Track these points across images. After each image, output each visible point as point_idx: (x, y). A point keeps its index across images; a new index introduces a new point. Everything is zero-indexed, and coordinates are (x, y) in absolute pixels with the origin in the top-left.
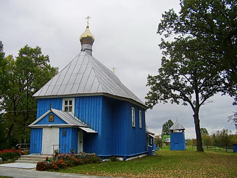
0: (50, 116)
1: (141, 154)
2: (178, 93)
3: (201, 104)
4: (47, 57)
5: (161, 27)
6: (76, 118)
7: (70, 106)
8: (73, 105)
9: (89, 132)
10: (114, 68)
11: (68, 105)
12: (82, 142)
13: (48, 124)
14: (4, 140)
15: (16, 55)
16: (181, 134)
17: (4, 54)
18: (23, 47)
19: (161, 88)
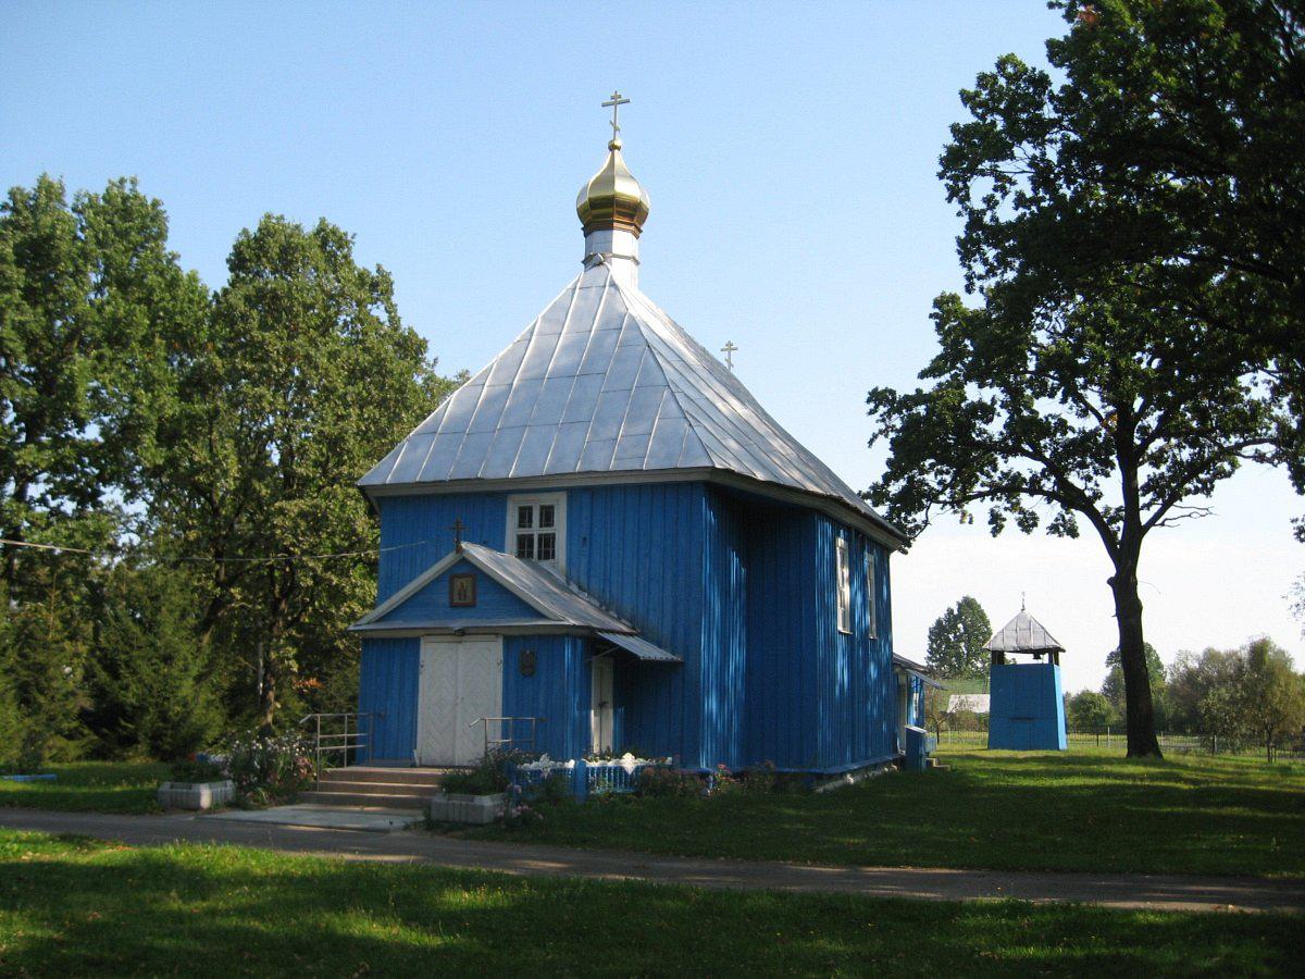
1: (468, 882)
2: (1025, 466)
3: (1152, 522)
6: (574, 588)
8: (560, 529)
10: (730, 347)
12: (610, 704)
16: (1040, 680)
19: (936, 444)
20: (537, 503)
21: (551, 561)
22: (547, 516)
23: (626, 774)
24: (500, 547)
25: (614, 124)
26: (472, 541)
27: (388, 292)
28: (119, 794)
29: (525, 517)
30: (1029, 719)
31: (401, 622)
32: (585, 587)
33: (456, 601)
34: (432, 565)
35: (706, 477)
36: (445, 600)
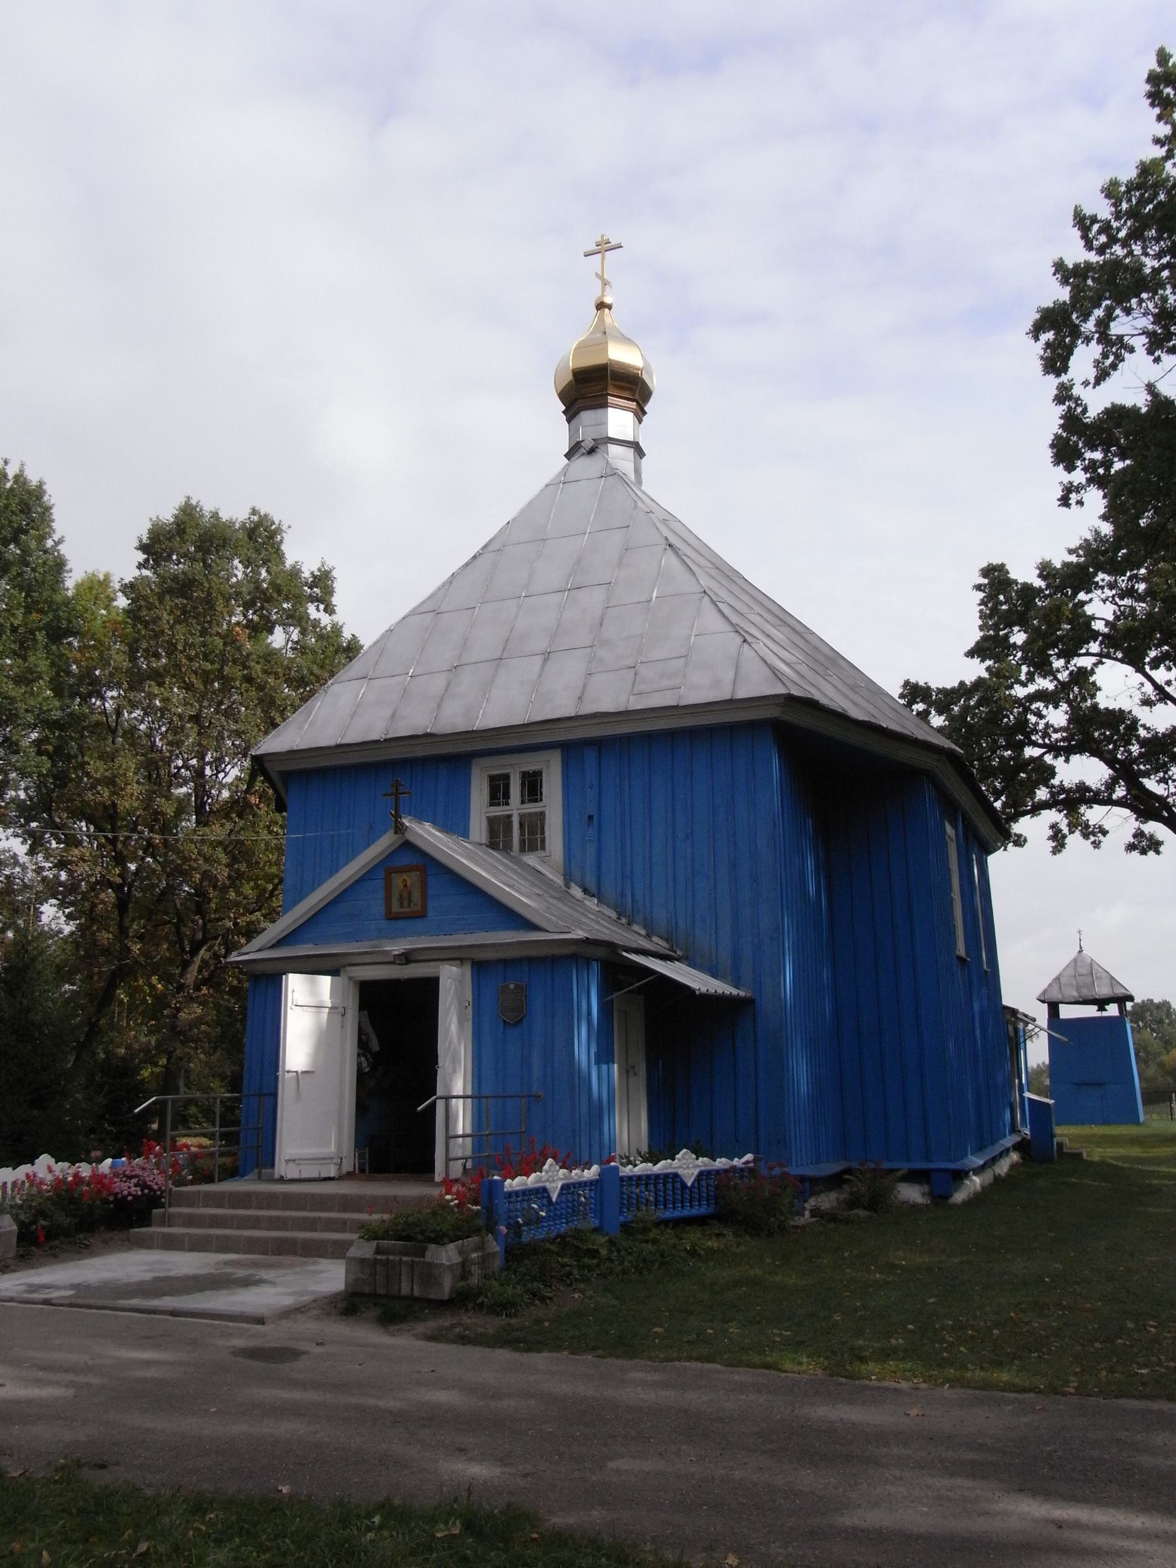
0: (398, 880)
4: (323, 581)
6: (577, 892)
7: (531, 808)
9: (704, 990)
11: (516, 807)
14: (53, 1075)
15: (124, 565)
17: (60, 565)
18: (167, 514)
20: (515, 769)
21: (540, 853)
22: (533, 787)
24: (464, 833)
25: (600, 277)
26: (420, 817)
27: (329, 591)
28: (479, 1118)
29: (498, 791)
30: (1101, 1084)
31: (310, 946)
32: (593, 889)
33: (396, 908)
35: (774, 713)
36: (379, 908)
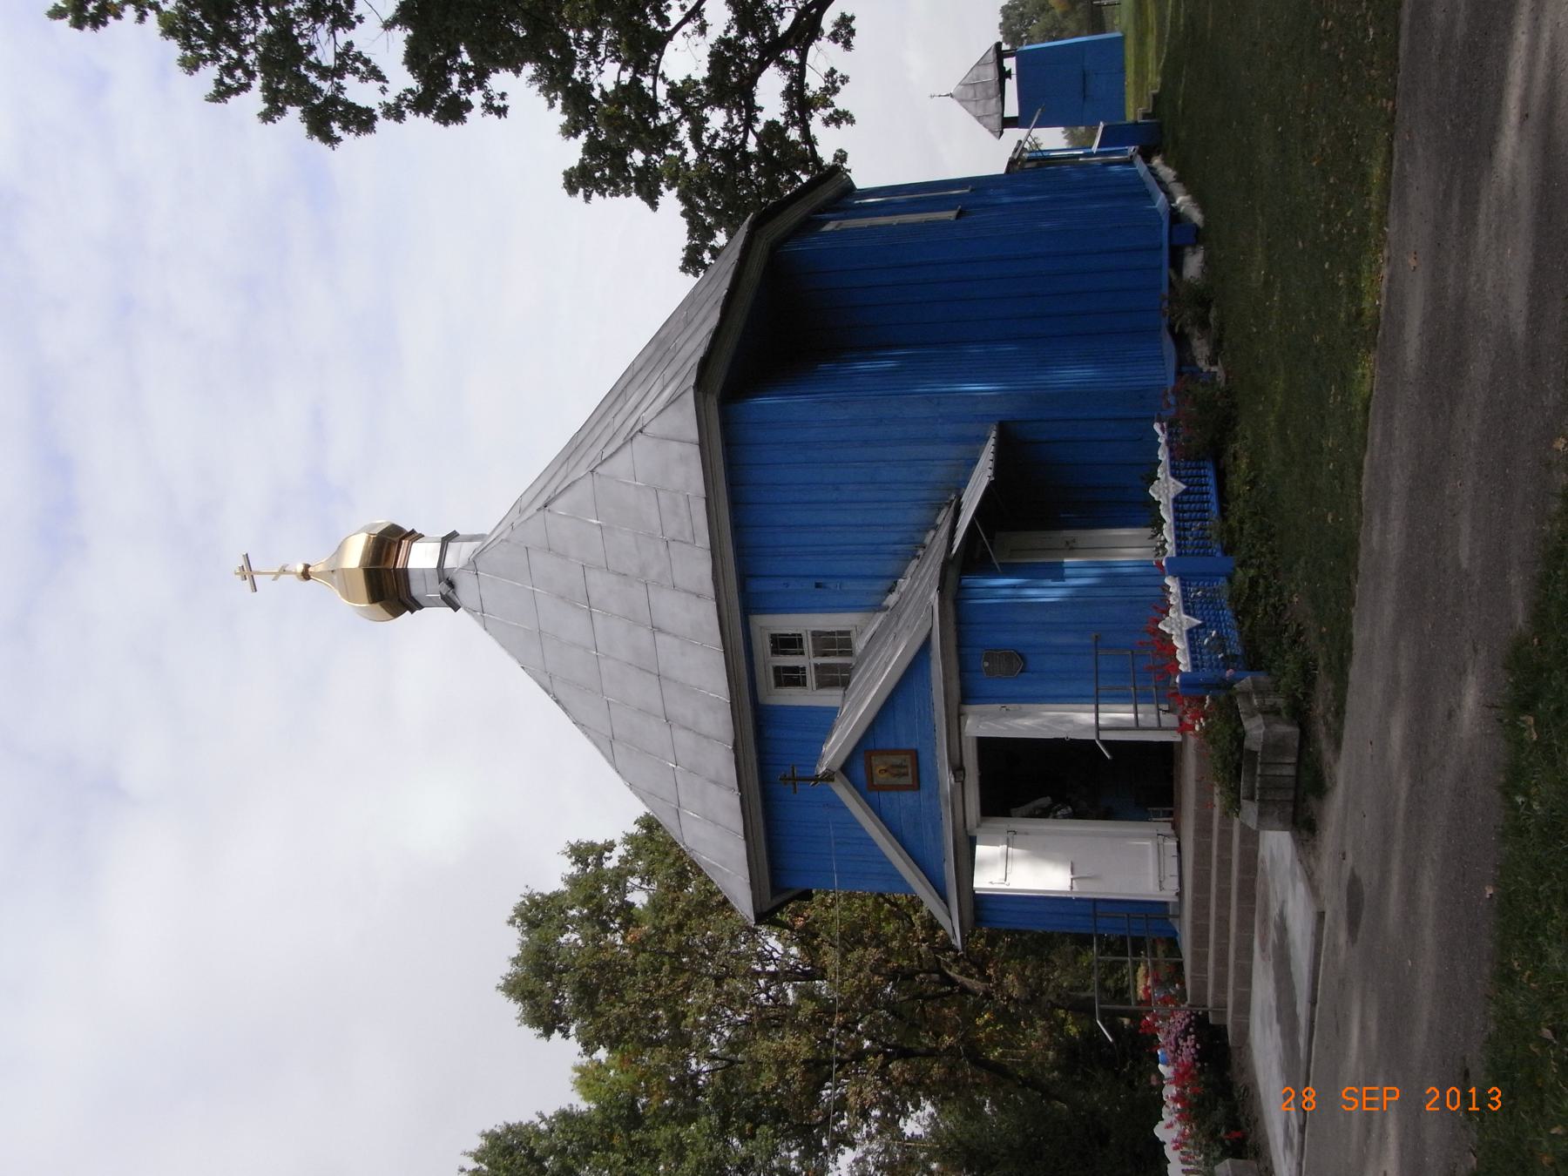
0: (881, 778)
2: (770, 90)
5: (330, 118)
6: (892, 599)
7: (808, 645)
9: (990, 472)
11: (807, 660)
13: (935, 792)
15: (564, 1054)
17: (565, 1117)
18: (514, 1009)
21: (853, 636)
23: (1185, 492)
25: (277, 575)
26: (818, 756)
27: (591, 847)
29: (791, 678)
32: (889, 583)
33: (908, 780)
34: (851, 815)
35: (713, 402)
36: (907, 798)
